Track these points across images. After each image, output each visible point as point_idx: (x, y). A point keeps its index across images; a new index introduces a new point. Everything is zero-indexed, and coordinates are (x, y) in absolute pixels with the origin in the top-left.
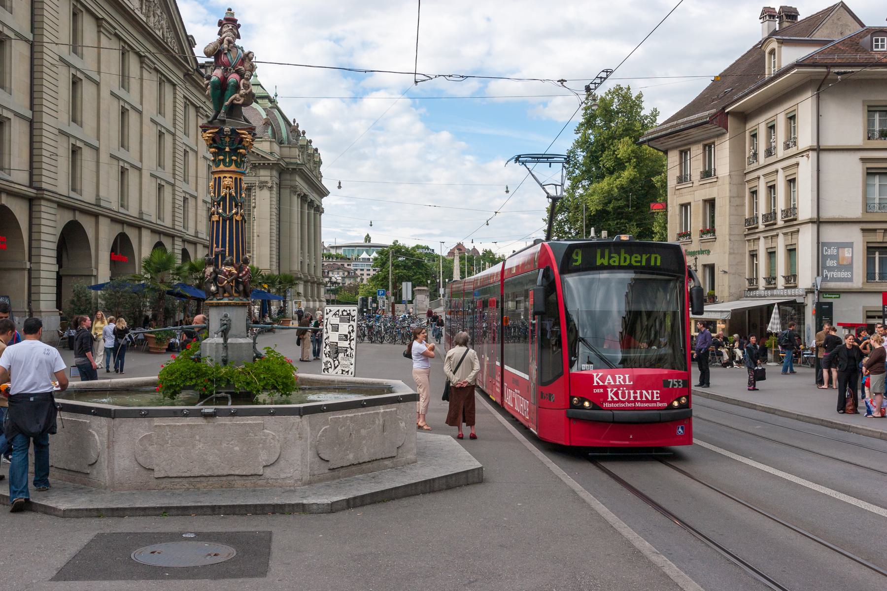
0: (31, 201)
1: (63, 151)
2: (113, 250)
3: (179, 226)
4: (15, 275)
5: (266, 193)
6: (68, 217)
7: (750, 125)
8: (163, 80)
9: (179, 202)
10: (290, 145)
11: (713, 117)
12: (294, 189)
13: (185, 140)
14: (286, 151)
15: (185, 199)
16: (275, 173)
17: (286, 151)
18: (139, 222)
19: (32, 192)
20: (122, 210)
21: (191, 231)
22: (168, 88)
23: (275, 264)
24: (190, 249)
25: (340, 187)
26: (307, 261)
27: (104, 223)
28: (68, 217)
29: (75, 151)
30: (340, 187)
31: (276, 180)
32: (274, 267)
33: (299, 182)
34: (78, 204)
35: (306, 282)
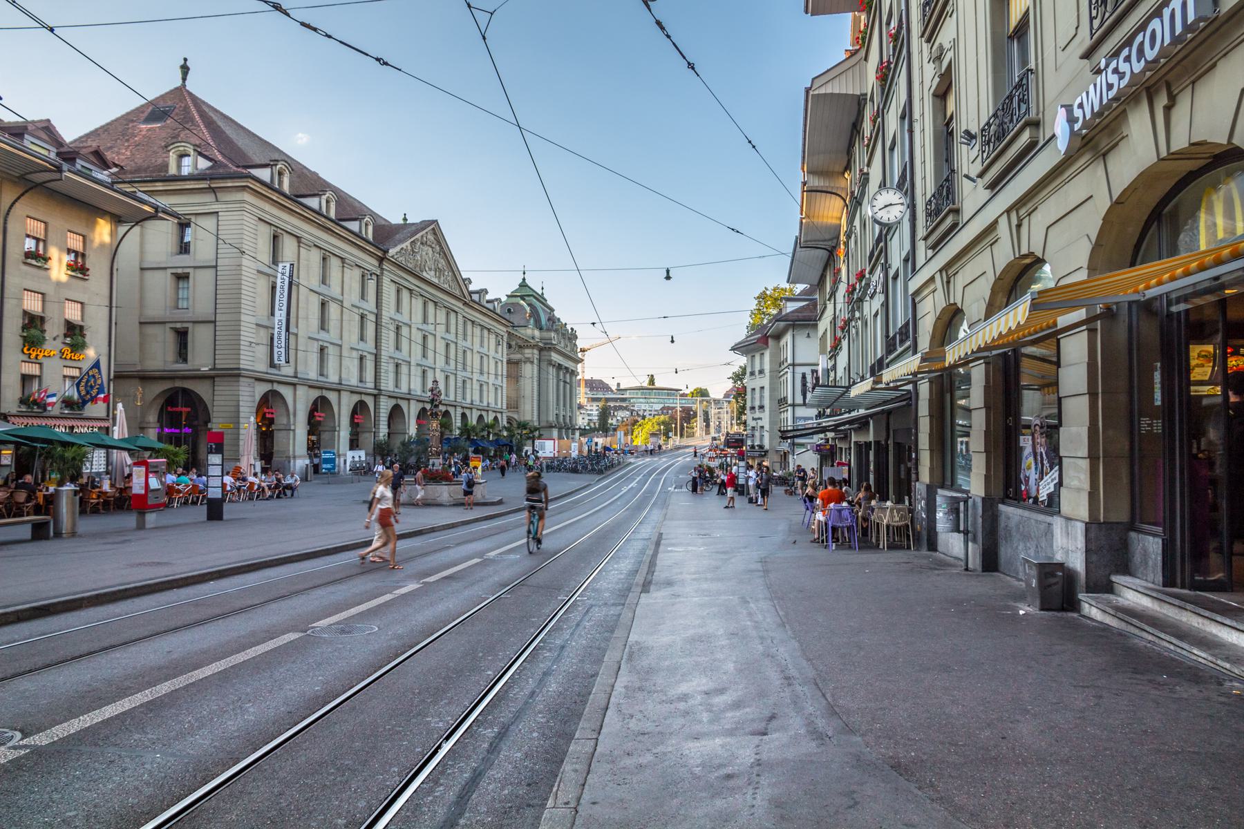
0: (376, 397)
1: (391, 368)
2: (418, 418)
3: (459, 399)
4: (367, 435)
5: (528, 366)
6: (393, 402)
7: (783, 342)
8: (449, 310)
9: (460, 384)
10: (548, 330)
11: (759, 340)
12: (550, 363)
13: (464, 344)
14: (545, 335)
15: (464, 382)
16: (536, 351)
17: (545, 335)
18: (339, 387)
19: (375, 392)
20: (321, 379)
21: (469, 401)
22: (453, 315)
23: (536, 413)
24: (468, 412)
25: (668, 278)
26: (562, 413)
27: (345, 395)
28: (420, 405)
29: (397, 365)
30: (668, 278)
31: (536, 356)
32: (535, 418)
33: (555, 357)
34: (327, 385)
35: (560, 429)
